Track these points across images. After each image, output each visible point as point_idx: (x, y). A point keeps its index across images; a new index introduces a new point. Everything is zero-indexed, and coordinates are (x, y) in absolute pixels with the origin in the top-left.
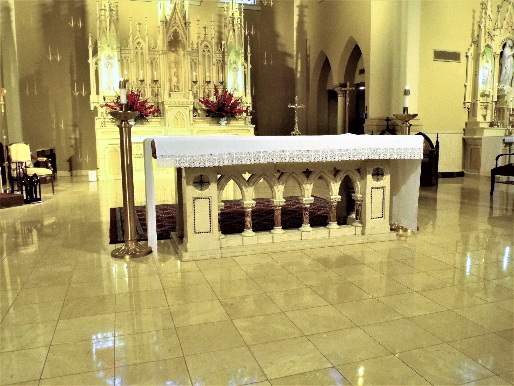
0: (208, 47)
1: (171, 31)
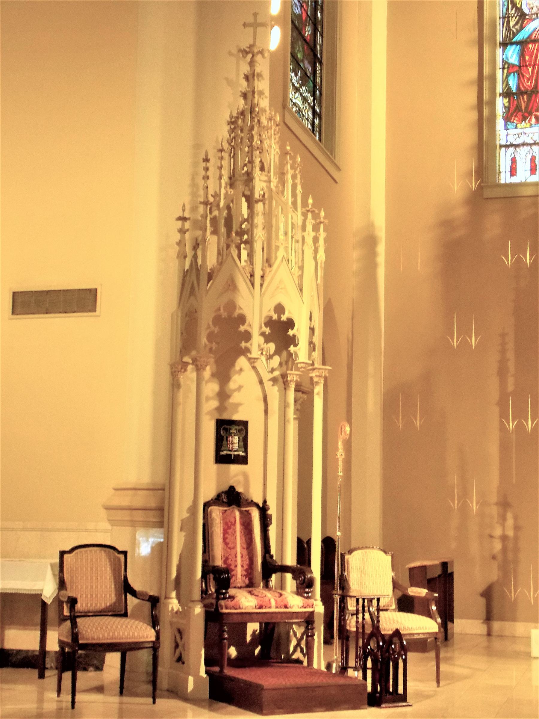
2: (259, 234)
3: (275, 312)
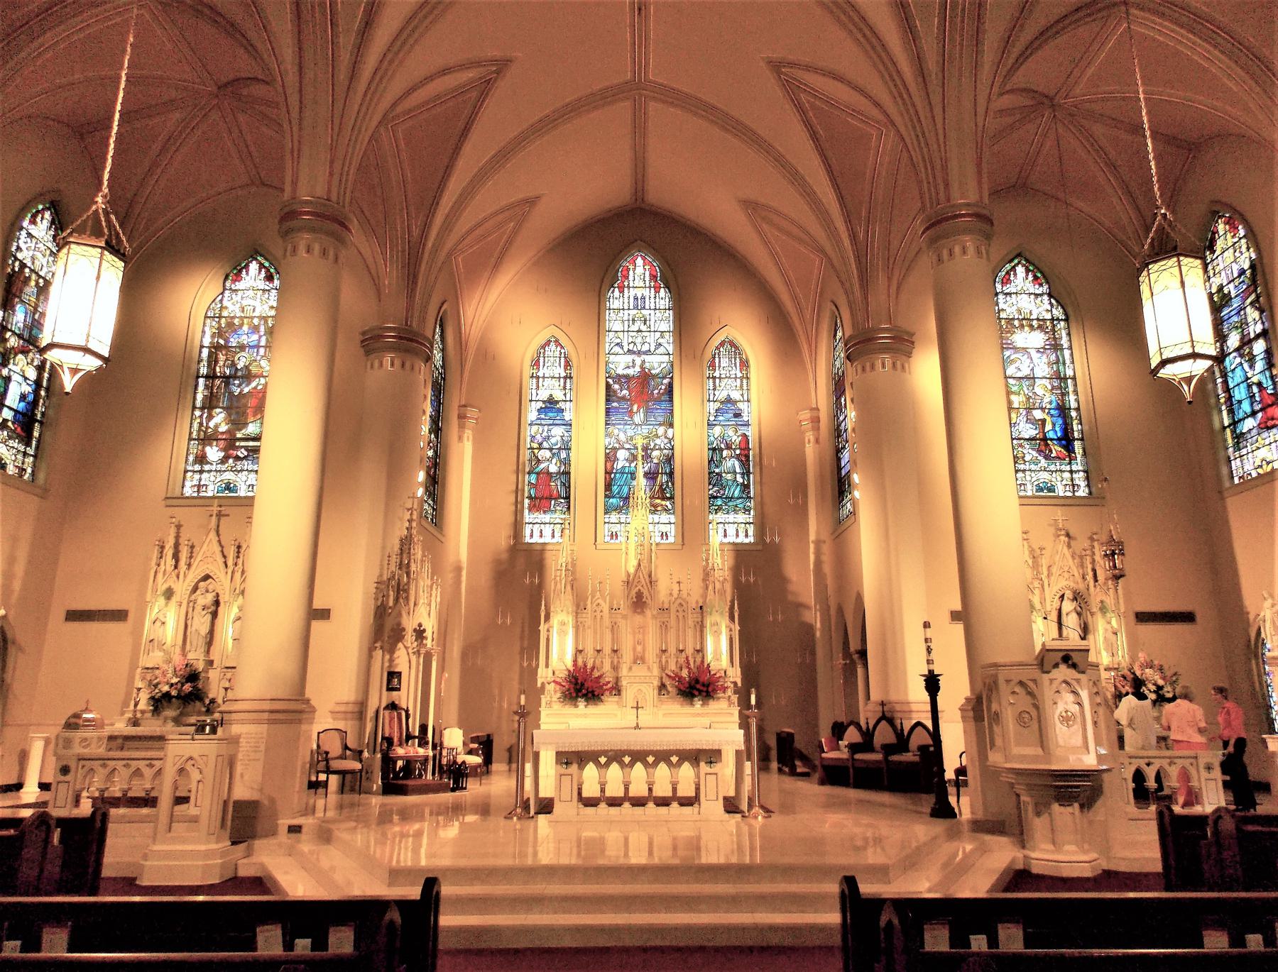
2: (412, 592)
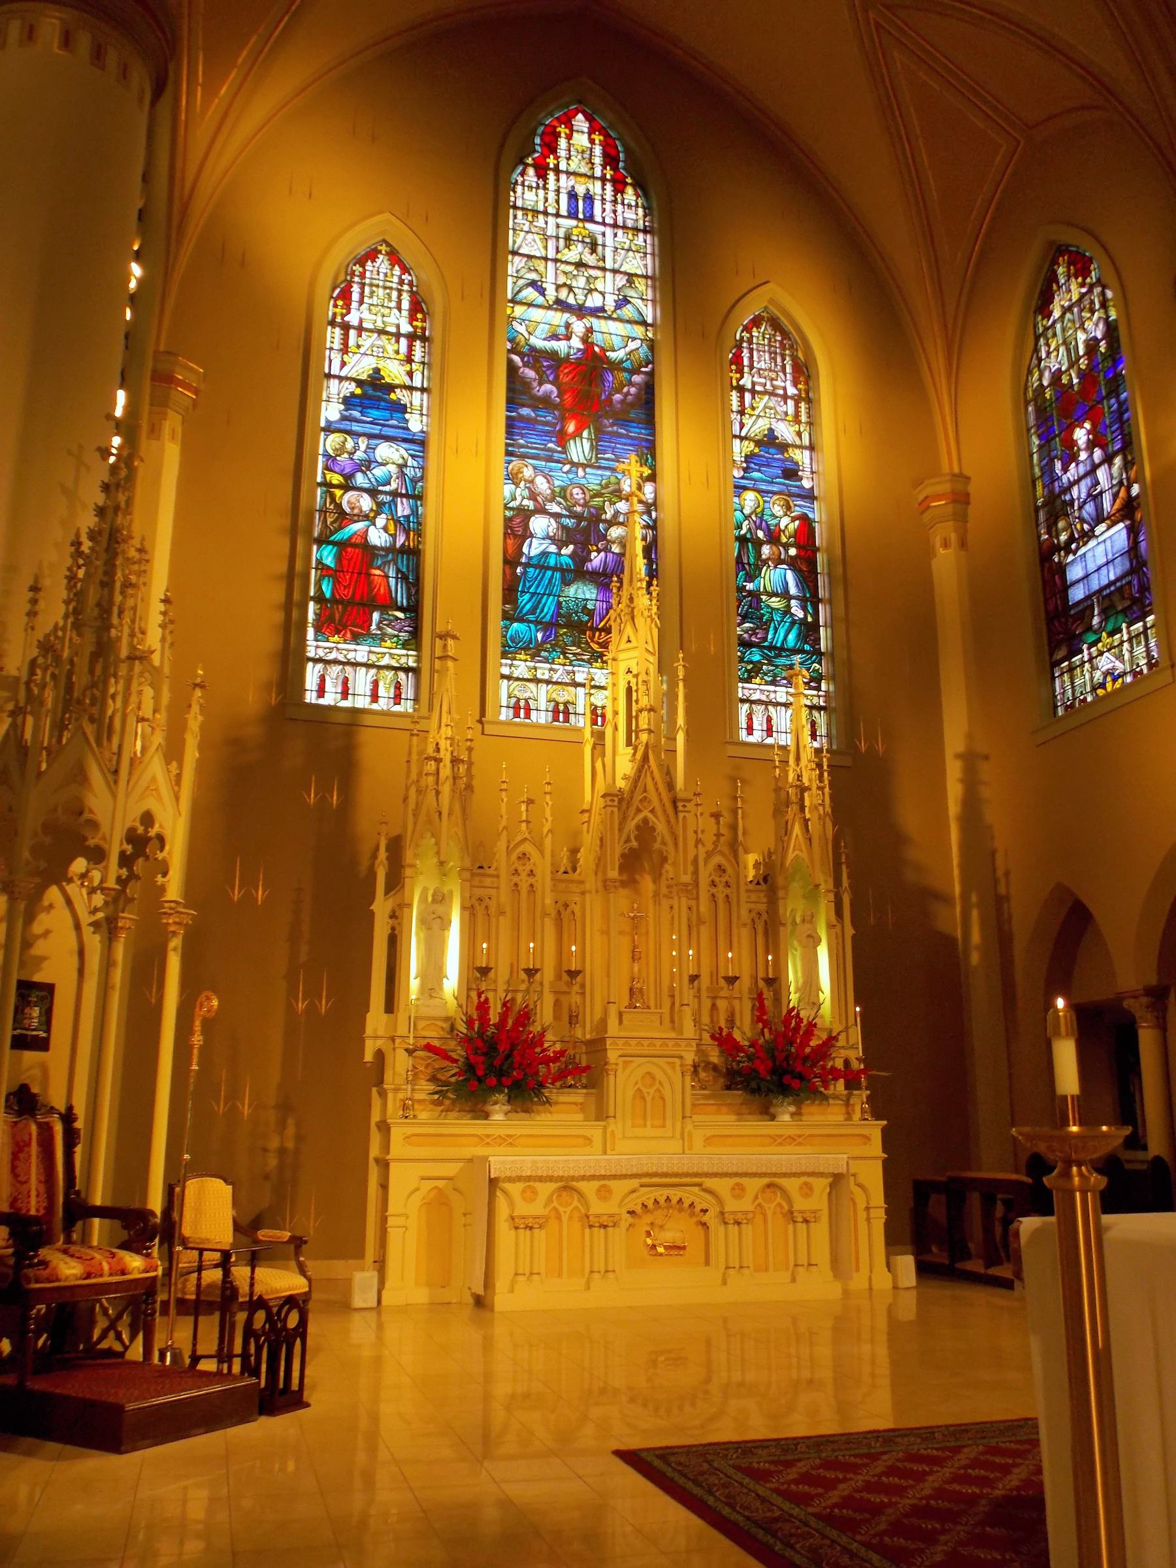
0: (724, 871)
1: (631, 825)
3: (142, 824)
